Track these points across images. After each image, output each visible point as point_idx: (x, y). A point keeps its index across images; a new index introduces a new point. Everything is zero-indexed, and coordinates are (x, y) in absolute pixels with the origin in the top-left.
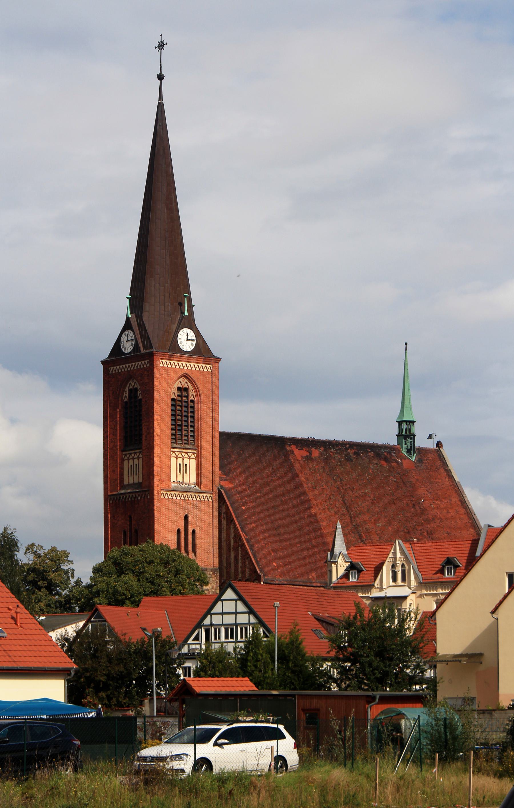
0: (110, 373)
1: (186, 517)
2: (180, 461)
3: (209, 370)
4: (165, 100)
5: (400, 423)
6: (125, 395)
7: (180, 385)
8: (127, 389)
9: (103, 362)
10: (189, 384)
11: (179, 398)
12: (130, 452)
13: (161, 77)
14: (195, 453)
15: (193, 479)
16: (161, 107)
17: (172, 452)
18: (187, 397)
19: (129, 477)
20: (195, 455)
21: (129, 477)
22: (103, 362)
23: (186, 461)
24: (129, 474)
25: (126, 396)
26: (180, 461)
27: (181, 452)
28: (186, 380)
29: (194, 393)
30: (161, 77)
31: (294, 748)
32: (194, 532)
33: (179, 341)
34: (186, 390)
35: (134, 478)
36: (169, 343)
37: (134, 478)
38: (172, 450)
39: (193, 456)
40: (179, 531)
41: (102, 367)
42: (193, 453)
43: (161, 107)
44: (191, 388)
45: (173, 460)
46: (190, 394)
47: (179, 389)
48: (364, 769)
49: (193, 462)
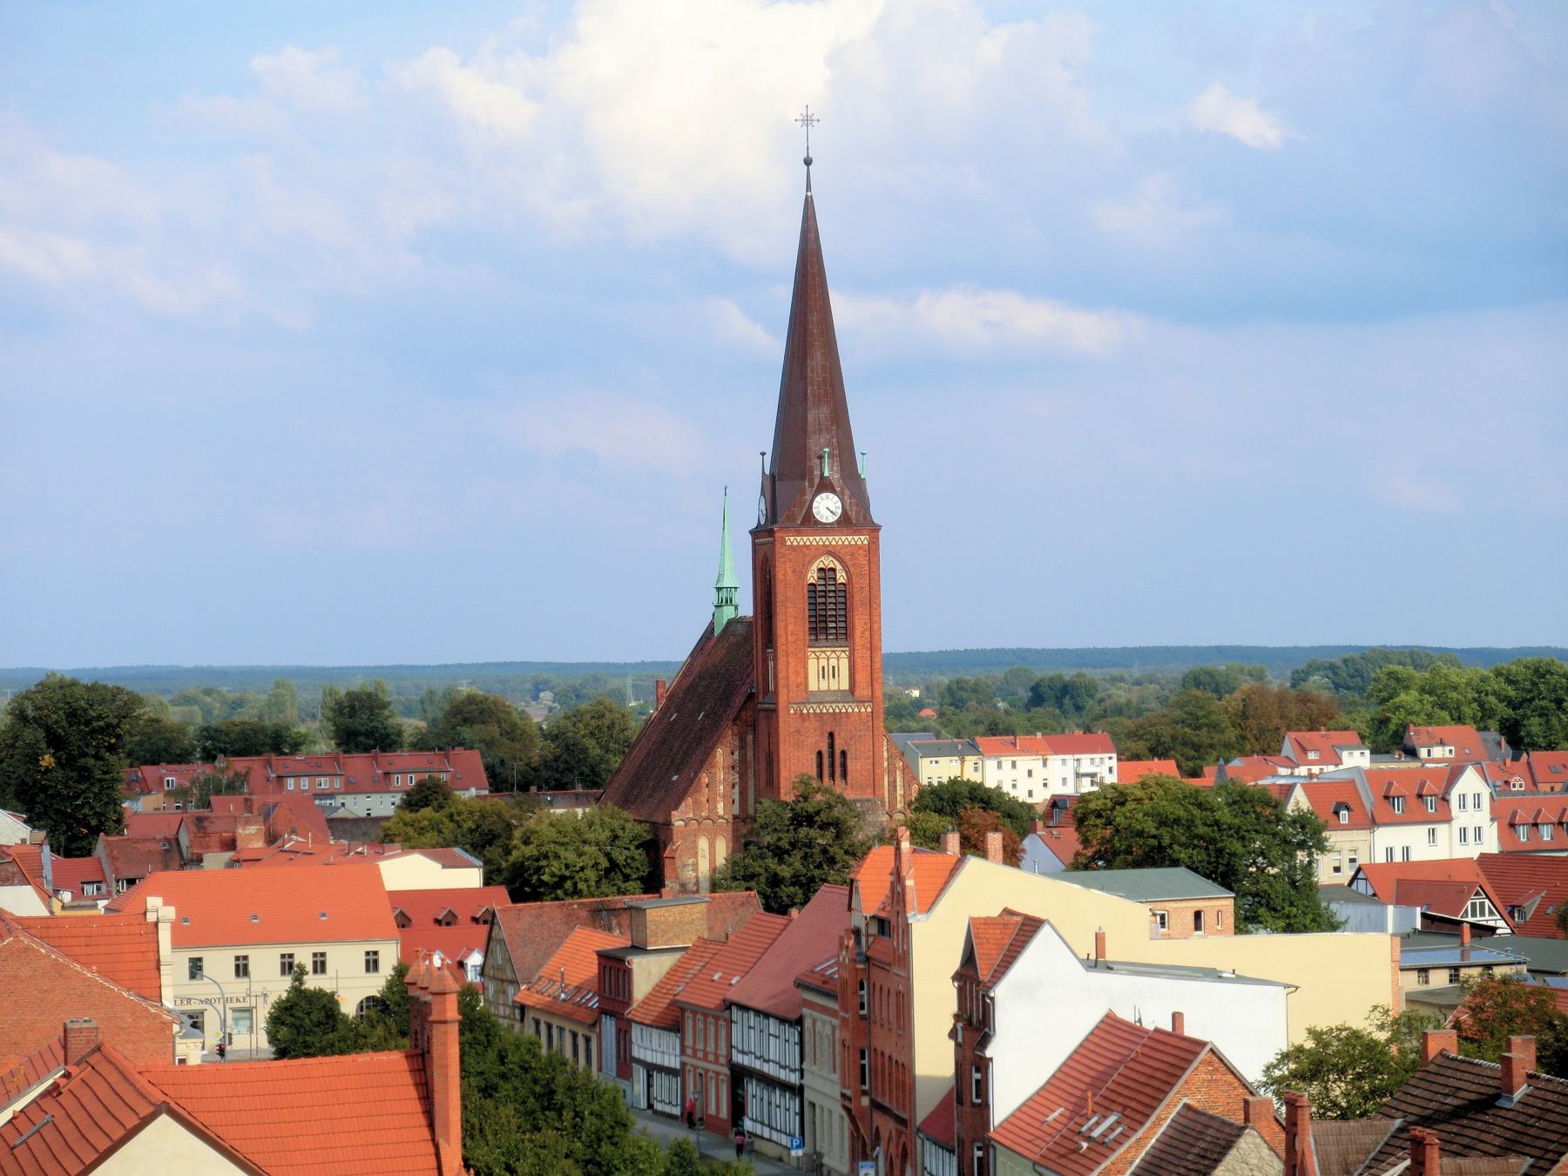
1: (831, 735)
2: (823, 662)
4: (814, 193)
5: (719, 589)
7: (822, 566)
9: (751, 532)
10: (836, 562)
11: (823, 582)
12: (824, 649)
13: (808, 162)
16: (809, 205)
18: (835, 579)
22: (751, 532)
26: (823, 662)
27: (824, 652)
28: (831, 558)
29: (844, 574)
30: (808, 162)
31: (991, 1059)
32: (844, 753)
33: (814, 511)
34: (833, 570)
36: (804, 510)
40: (820, 754)
41: (750, 538)
43: (809, 205)
44: (839, 567)
46: (838, 575)
47: (821, 570)
48: (570, 1162)
49: (844, 664)
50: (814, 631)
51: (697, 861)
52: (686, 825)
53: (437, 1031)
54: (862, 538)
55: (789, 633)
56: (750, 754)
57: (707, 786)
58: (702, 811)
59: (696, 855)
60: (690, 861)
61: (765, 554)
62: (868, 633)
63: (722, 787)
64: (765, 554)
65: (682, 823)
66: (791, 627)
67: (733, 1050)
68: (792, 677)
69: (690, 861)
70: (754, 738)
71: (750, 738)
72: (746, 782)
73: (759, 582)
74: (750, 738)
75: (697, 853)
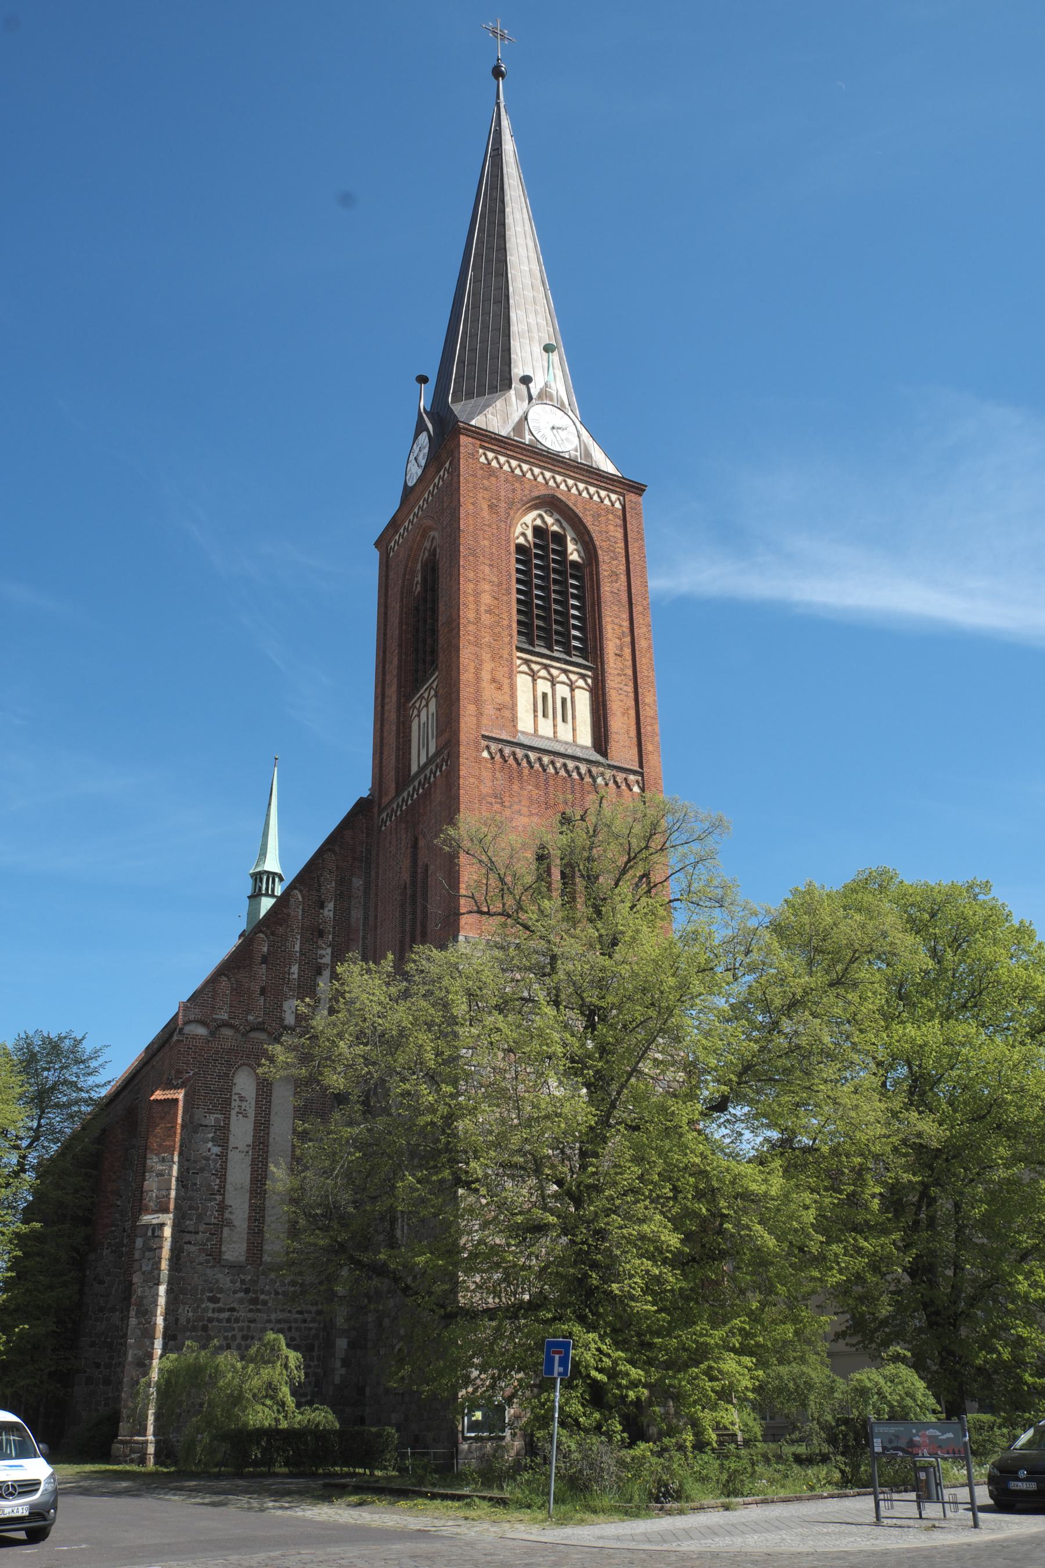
0: (392, 554)
3: (618, 505)
6: (416, 579)
7: (539, 522)
8: (419, 567)
10: (565, 524)
14: (588, 676)
15: (585, 738)
17: (519, 662)
19: (535, 716)
20: (589, 681)
21: (535, 716)
23: (563, 691)
24: (535, 711)
25: (417, 583)
26: (544, 686)
35: (555, 726)
37: (555, 726)
38: (519, 654)
39: (581, 683)
42: (583, 677)
45: (523, 682)
49: (583, 700)
50: (526, 629)
51: (228, 1118)
52: (212, 1034)
53: (167, 1257)
54: (614, 497)
55: (483, 608)
56: (357, 914)
57: (265, 960)
58: (248, 1012)
59: (225, 1107)
60: (211, 1120)
61: (433, 553)
62: (627, 651)
63: (295, 969)
64: (433, 553)
65: (201, 1031)
66: (486, 599)
67: (410, 484)
68: (488, 691)
69: (211, 1120)
70: (367, 890)
71: (358, 882)
72: (425, 579)
73: (393, 645)
74: (358, 882)
75: (228, 1102)
